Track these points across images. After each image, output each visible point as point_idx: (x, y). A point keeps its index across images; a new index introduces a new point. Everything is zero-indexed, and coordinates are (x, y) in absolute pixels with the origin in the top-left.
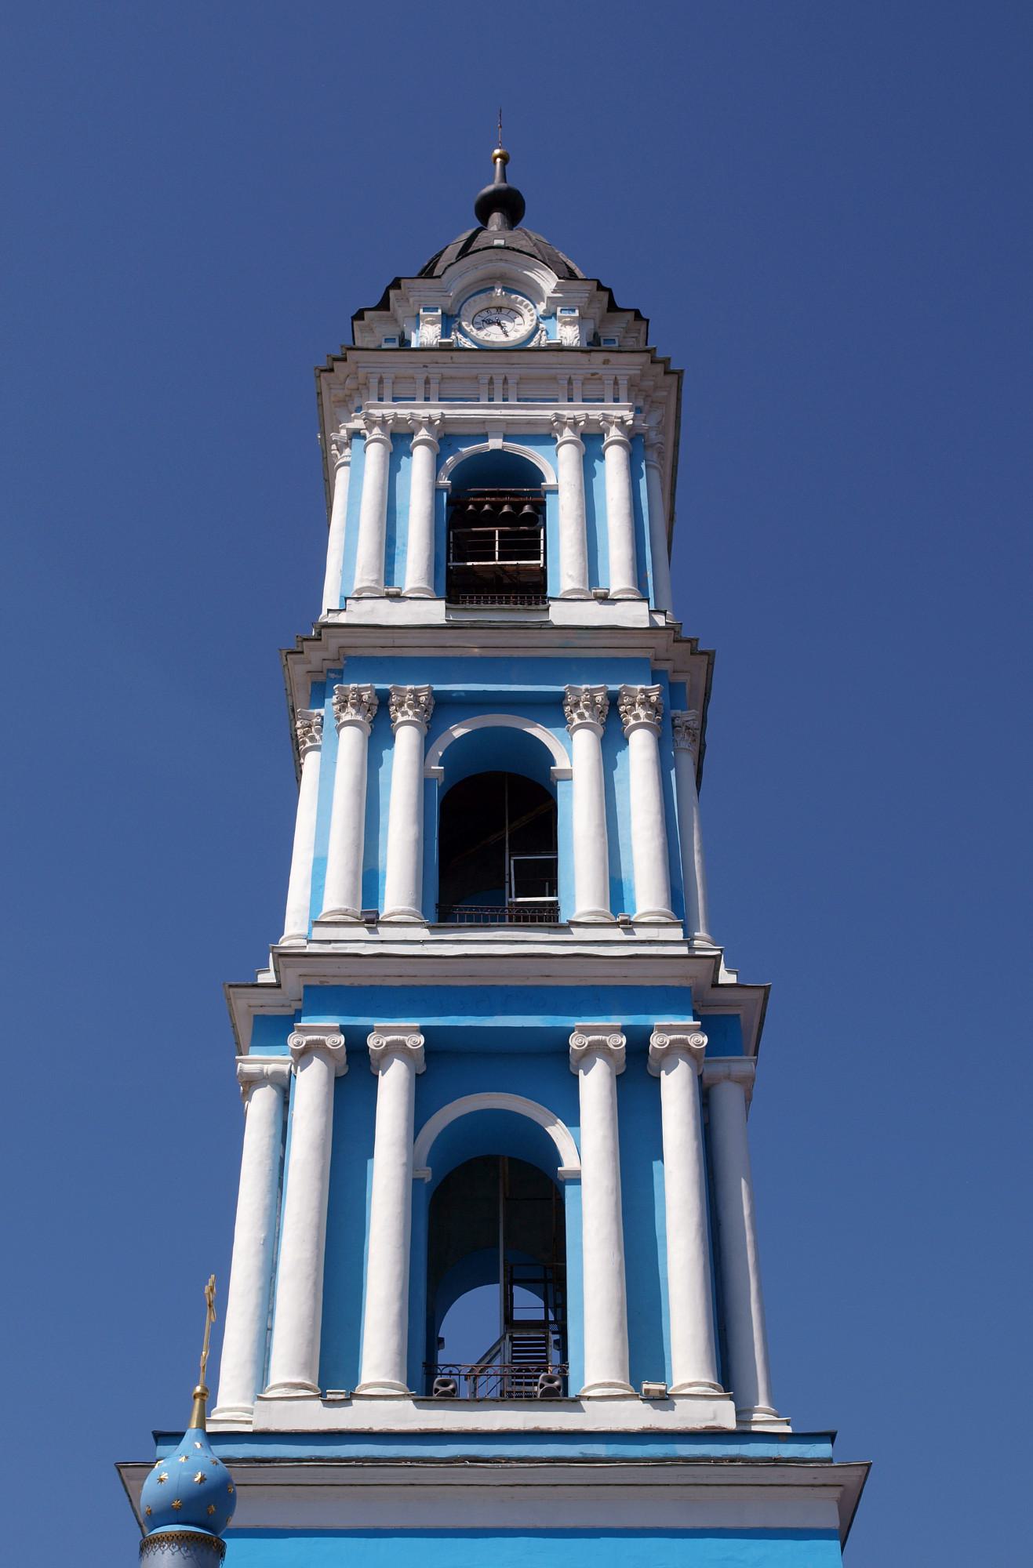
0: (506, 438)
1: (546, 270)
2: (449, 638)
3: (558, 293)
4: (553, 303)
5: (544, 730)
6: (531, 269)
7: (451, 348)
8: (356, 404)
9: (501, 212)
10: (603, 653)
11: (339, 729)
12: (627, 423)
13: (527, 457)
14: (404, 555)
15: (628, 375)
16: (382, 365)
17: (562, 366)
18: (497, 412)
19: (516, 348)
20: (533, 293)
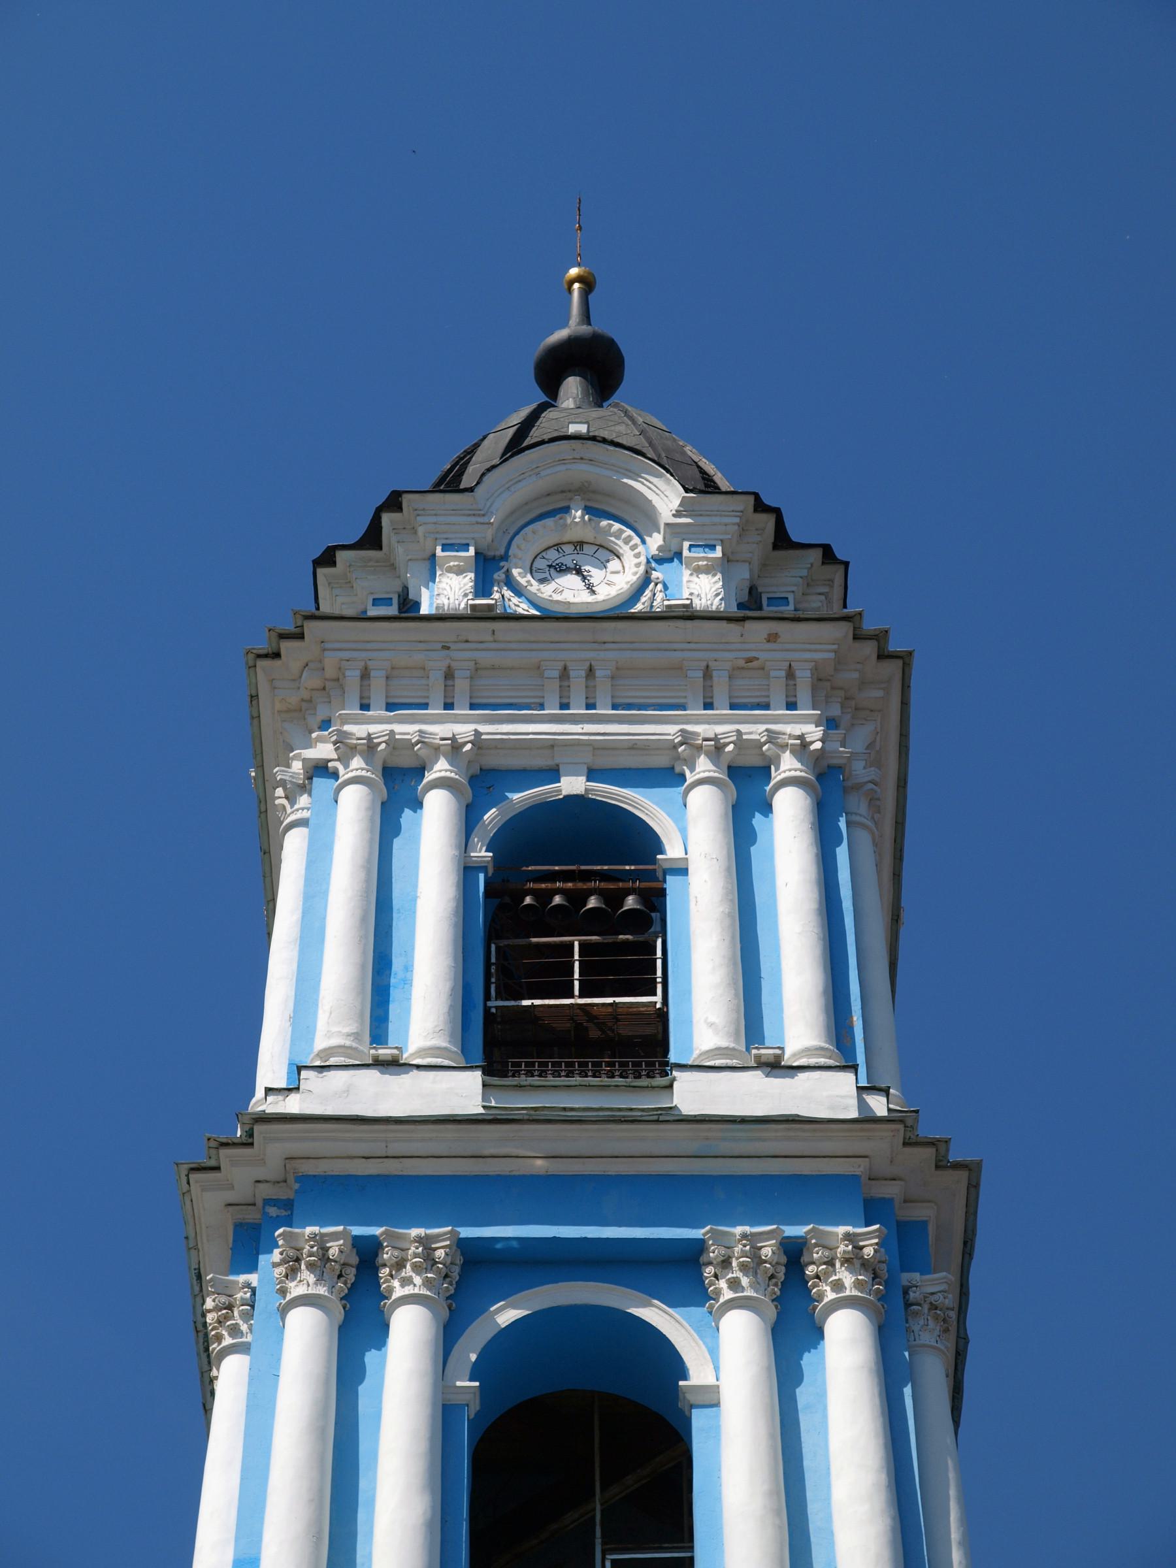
0: (593, 774)
2: (490, 1139)
3: (685, 516)
6: (635, 476)
19: (611, 614)
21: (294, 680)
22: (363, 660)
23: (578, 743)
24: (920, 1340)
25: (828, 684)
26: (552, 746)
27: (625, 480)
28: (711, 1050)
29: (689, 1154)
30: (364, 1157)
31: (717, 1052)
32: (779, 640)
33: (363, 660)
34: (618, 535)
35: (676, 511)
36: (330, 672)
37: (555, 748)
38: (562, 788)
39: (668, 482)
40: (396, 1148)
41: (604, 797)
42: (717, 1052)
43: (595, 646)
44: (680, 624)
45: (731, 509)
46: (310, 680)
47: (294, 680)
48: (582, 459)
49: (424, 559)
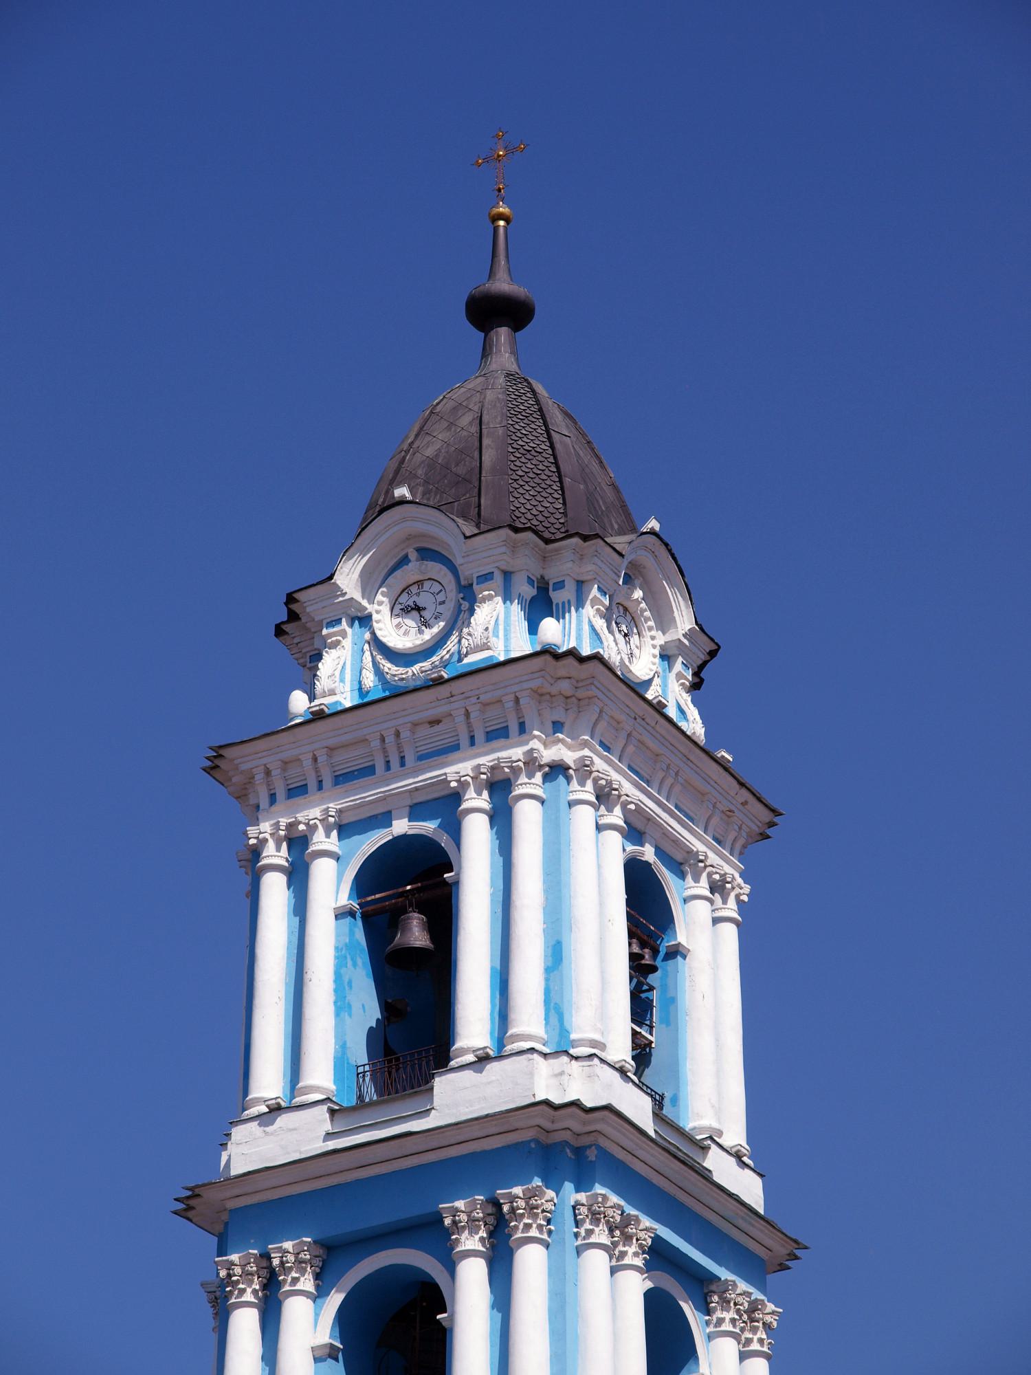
0: (659, 852)
1: (686, 602)
2: (758, 1230)
3: (688, 640)
4: (678, 647)
5: (692, 1310)
6: (671, 585)
7: (660, 710)
8: (559, 715)
9: (509, 327)
10: (752, 1245)
11: (579, 1251)
12: (600, 782)
13: (663, 883)
14: (560, 967)
15: (750, 828)
16: (605, 691)
17: (715, 785)
18: (664, 815)
19: (632, 685)
20: (664, 621)
21: (552, 677)
22: (678, 767)
23: (660, 826)
24: (710, 1337)
25: (574, 699)
26: (649, 820)
27: (664, 582)
28: (716, 1129)
29: (768, 1247)
30: (621, 1147)
31: (718, 1132)
32: (746, 806)
33: (678, 767)
34: (647, 620)
35: (686, 633)
36: (580, 694)
37: (650, 823)
38: (646, 853)
39: (687, 607)
40: (639, 1153)
41: (662, 878)
42: (718, 1132)
43: (685, 759)
44: (721, 770)
45: (704, 648)
46: (565, 686)
47: (552, 677)
48: (653, 552)
49: (574, 579)
